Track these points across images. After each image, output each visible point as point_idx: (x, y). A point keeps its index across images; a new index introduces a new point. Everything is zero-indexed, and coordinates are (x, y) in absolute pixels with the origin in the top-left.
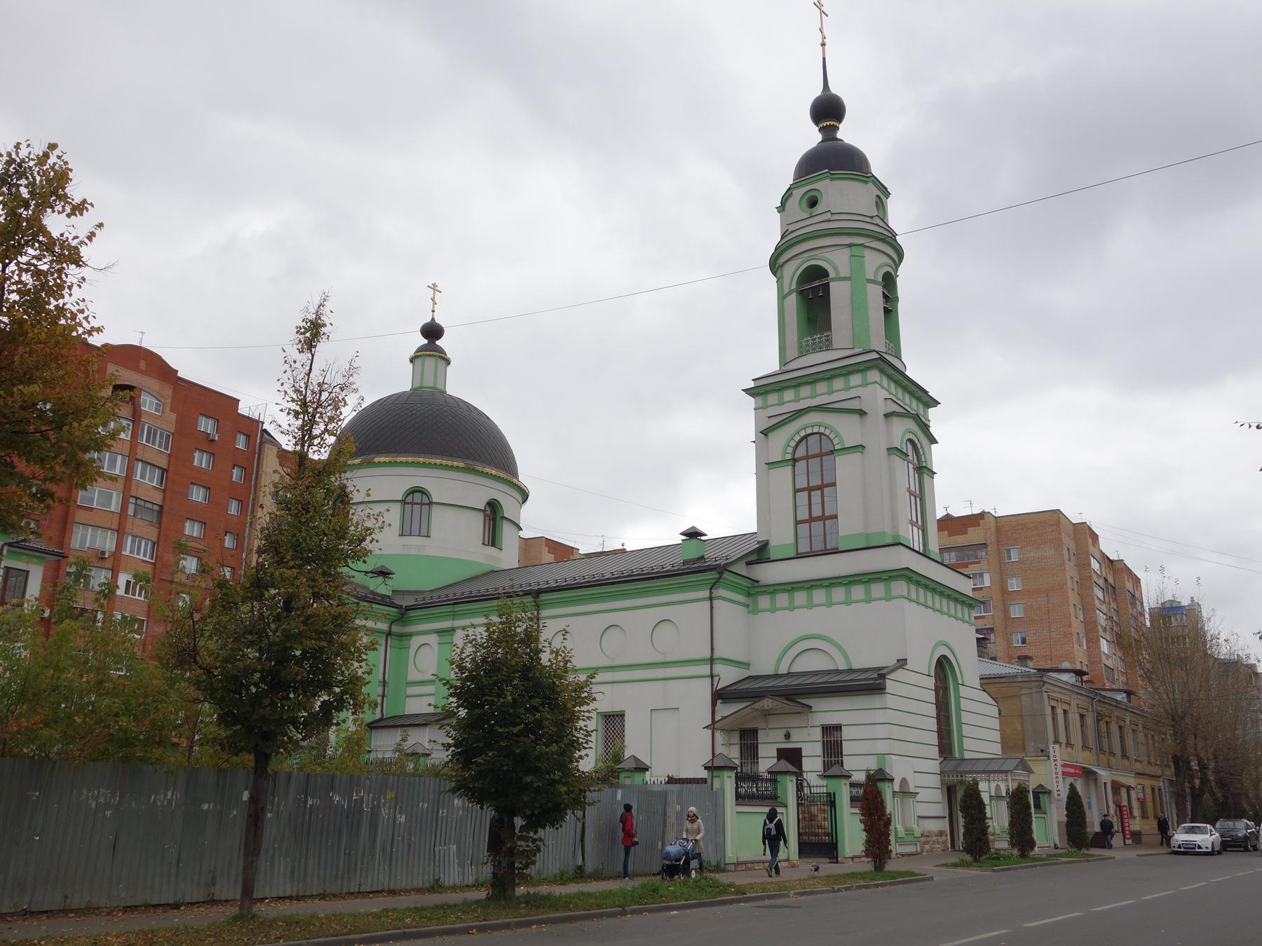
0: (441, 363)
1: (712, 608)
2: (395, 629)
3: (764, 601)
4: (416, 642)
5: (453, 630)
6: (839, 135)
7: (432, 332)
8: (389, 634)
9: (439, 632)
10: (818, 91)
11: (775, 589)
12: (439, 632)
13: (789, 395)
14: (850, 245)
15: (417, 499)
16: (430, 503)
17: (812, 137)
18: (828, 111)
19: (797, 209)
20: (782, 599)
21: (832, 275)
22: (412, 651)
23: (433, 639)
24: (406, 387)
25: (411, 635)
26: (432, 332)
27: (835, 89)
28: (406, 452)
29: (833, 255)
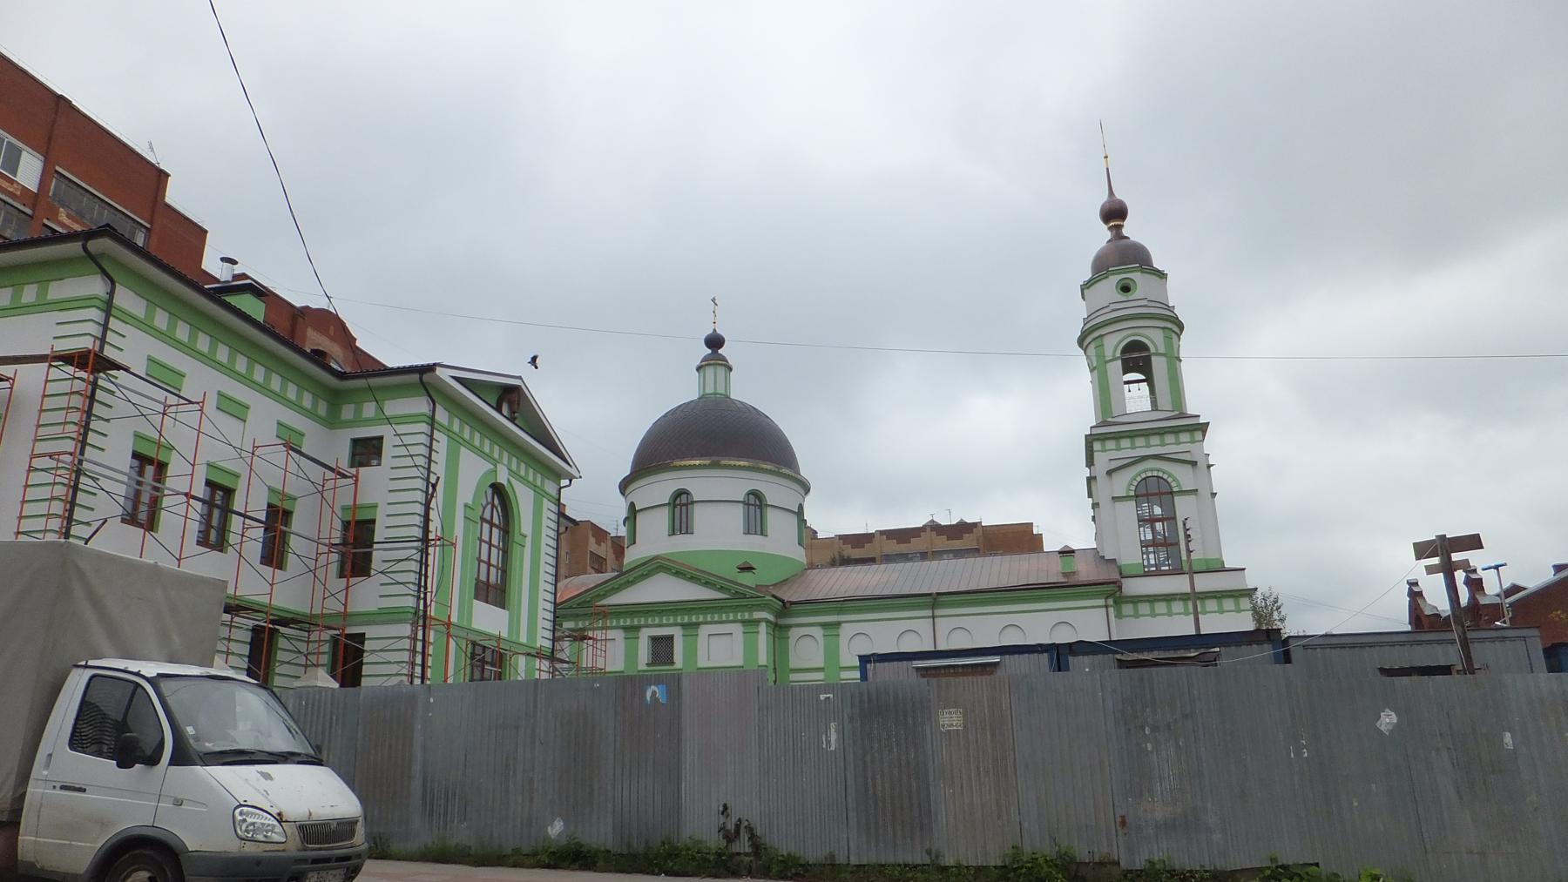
0: (721, 371)
1: (128, 708)
3: (1127, 609)
4: (794, 633)
5: (838, 624)
6: (1125, 232)
7: (715, 342)
9: (824, 625)
10: (1105, 197)
11: (1136, 600)
12: (824, 625)
13: (1140, 441)
14: (1164, 328)
15: (681, 503)
16: (1171, 493)
17: (1102, 235)
18: (1114, 214)
19: (1108, 289)
20: (1144, 608)
21: (1153, 350)
22: (792, 642)
23: (818, 632)
24: (694, 395)
25: (790, 626)
26: (715, 342)
27: (1119, 195)
28: (739, 457)
29: (1132, 328)
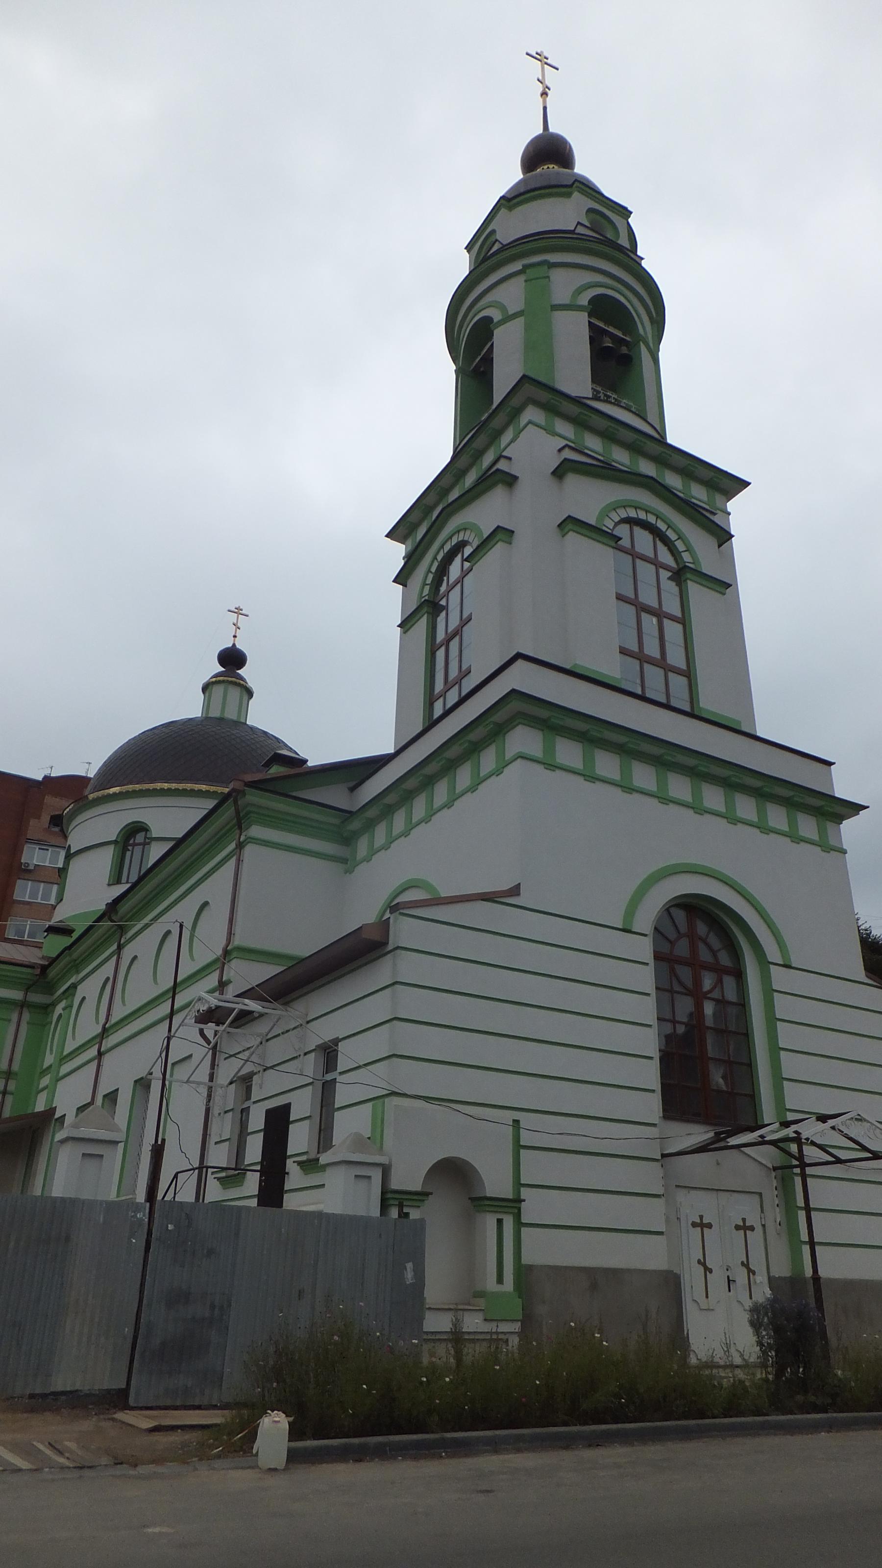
2: (36, 998)
8: (22, 1005)
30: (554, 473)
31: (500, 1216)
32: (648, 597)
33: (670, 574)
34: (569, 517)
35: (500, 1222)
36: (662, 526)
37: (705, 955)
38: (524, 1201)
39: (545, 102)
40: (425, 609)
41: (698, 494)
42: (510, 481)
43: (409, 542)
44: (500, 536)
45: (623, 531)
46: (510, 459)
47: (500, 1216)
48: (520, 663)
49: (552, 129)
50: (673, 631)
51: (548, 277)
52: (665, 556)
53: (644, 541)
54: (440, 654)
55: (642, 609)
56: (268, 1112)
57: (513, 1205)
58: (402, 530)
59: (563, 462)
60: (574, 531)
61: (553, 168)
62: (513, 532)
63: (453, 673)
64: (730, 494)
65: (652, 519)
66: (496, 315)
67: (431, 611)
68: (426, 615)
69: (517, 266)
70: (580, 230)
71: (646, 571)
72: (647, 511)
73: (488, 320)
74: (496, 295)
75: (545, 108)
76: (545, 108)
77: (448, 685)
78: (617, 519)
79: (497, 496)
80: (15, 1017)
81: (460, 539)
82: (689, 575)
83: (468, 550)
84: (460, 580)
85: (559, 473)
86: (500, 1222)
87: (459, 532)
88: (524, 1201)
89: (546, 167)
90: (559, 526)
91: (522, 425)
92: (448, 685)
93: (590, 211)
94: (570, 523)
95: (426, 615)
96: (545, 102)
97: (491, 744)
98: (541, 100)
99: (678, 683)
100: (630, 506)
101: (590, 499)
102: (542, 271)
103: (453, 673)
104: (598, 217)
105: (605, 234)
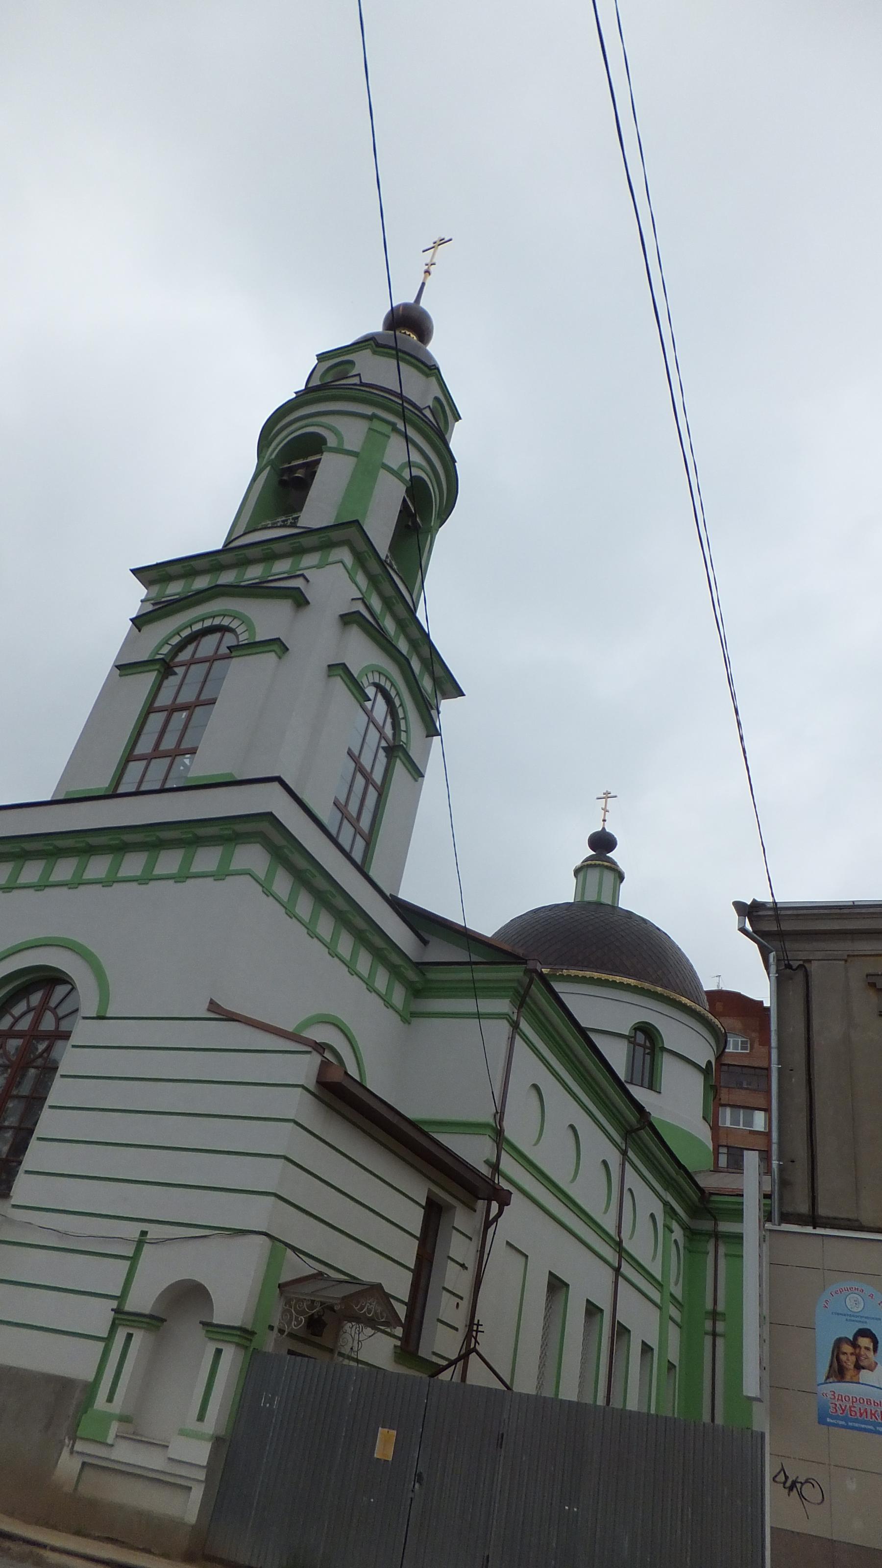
30: (342, 616)
31: (219, 1346)
32: (366, 761)
33: (386, 745)
34: (344, 665)
35: (219, 1352)
36: (397, 702)
37: (24, 1025)
38: (112, 1310)
39: (425, 278)
40: (157, 667)
41: (427, 684)
42: (300, 600)
43: (156, 589)
44: (275, 647)
45: (371, 691)
46: (308, 581)
47: (219, 1346)
48: (276, 785)
49: (423, 304)
50: (372, 794)
51: (389, 437)
52: (388, 731)
53: (380, 708)
54: (156, 721)
55: (359, 768)
56: (601, 1311)
57: (122, 1317)
58: (153, 574)
59: (354, 612)
60: (342, 678)
61: (414, 337)
62: (287, 649)
63: (168, 743)
64: (446, 696)
65: (393, 693)
66: (332, 441)
67: (162, 670)
68: (155, 673)
69: (369, 410)
70: (427, 413)
71: (373, 734)
72: (392, 684)
73: (322, 440)
74: (341, 423)
75: (423, 284)
76: (423, 284)
77: (156, 753)
78: (377, 681)
79: (283, 608)
80: (711, 1247)
81: (223, 623)
82: (400, 754)
83: (229, 640)
84: (211, 660)
85: (347, 619)
86: (219, 1352)
87: (224, 616)
88: (112, 1310)
89: (408, 333)
90: (329, 666)
91: (330, 560)
92: (156, 753)
93: (437, 399)
94: (338, 669)
95: (155, 673)
96: (425, 278)
97: (218, 845)
98: (423, 275)
99: (360, 843)
100: (384, 675)
101: (361, 654)
102: (386, 429)
103: (168, 743)
104: (439, 408)
105: (433, 421)
